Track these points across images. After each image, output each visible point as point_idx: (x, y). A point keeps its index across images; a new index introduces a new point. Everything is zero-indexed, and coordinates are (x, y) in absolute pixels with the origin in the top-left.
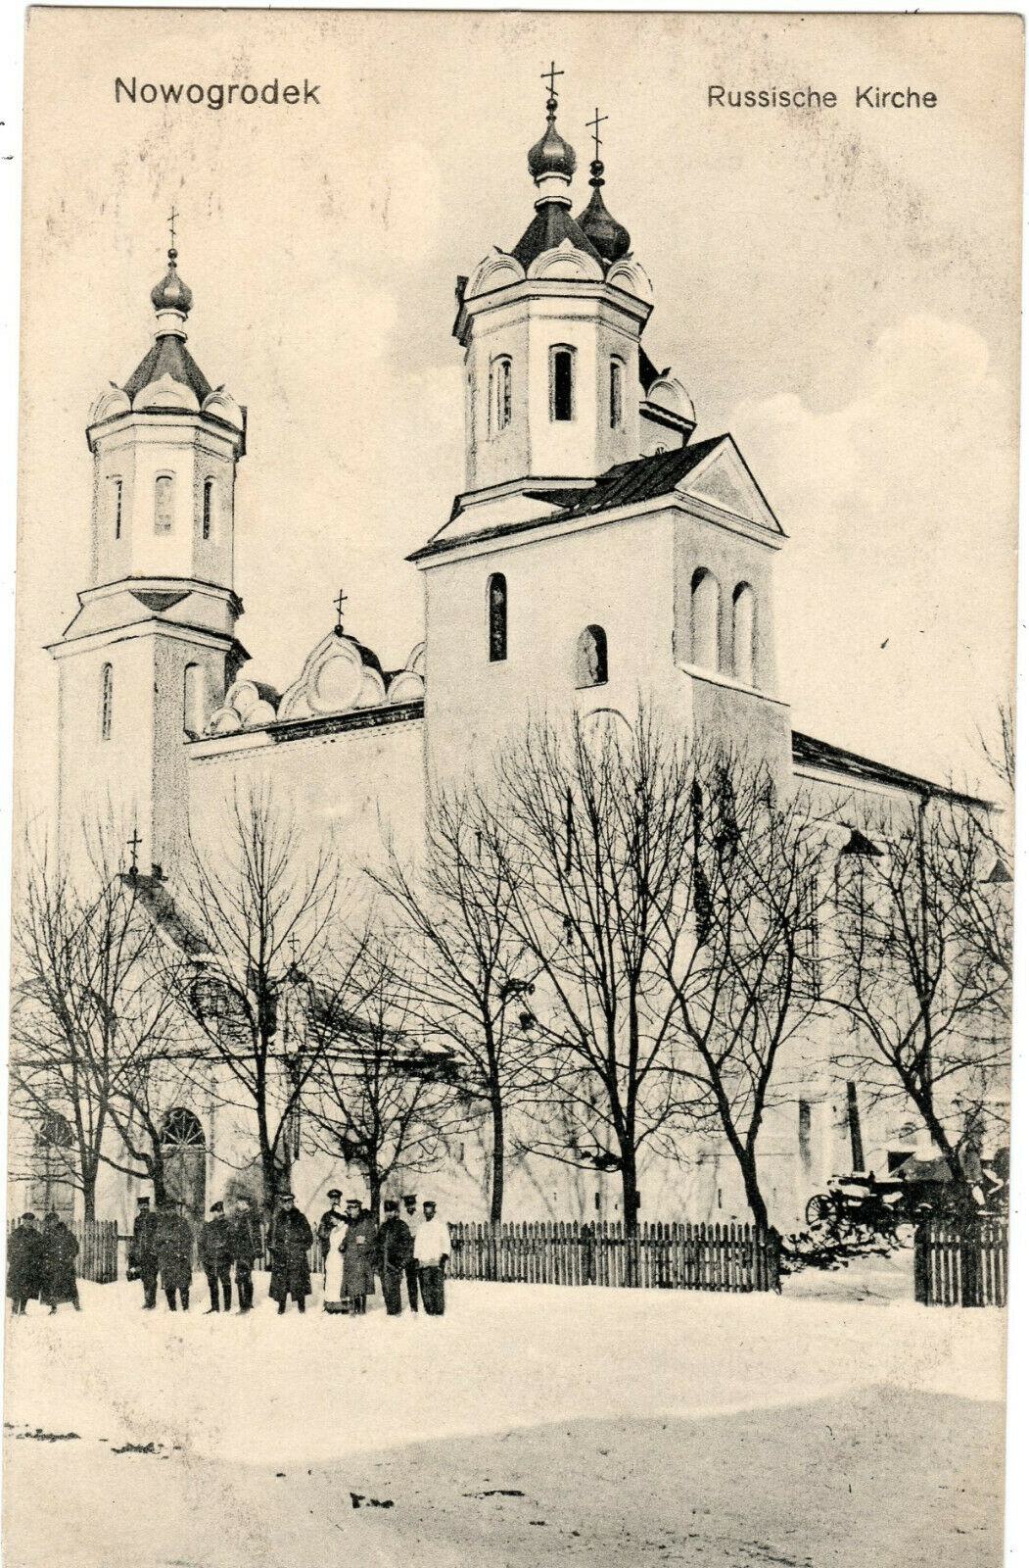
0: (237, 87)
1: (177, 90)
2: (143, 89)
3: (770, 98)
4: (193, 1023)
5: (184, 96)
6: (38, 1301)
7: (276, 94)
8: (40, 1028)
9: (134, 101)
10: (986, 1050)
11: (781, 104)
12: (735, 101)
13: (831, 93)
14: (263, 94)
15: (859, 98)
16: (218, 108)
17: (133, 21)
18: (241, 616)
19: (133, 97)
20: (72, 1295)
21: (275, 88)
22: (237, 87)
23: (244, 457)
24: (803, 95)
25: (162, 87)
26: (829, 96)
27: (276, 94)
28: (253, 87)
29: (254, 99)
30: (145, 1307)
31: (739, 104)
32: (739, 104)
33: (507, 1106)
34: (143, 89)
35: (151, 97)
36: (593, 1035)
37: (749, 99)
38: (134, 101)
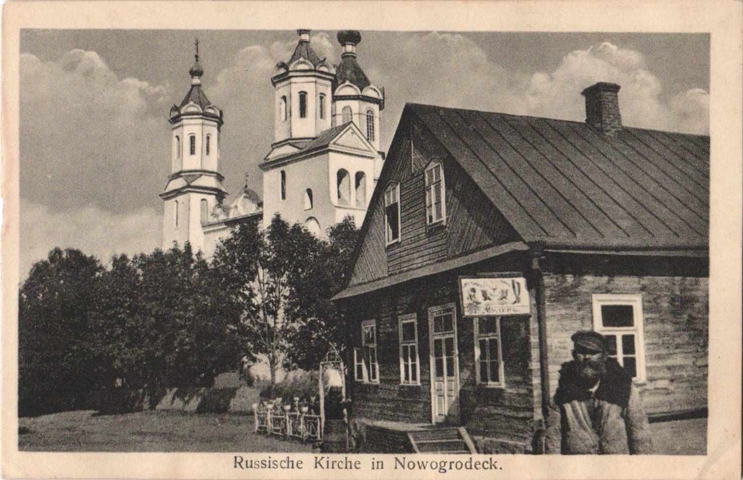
1: (425, 464)
2: (408, 464)
3: (267, 464)
5: (428, 467)
6: (130, 257)
7: (471, 466)
9: (404, 468)
10: (234, 214)
11: (273, 467)
12: (249, 465)
15: (316, 463)
17: (734, 436)
19: (403, 467)
20: (115, 261)
22: (453, 462)
24: (487, 463)
25: (418, 462)
26: (478, 463)
27: (471, 466)
29: (461, 467)
30: (278, 216)
31: (471, 468)
32: (451, 463)
34: (408, 464)
37: (275, 464)
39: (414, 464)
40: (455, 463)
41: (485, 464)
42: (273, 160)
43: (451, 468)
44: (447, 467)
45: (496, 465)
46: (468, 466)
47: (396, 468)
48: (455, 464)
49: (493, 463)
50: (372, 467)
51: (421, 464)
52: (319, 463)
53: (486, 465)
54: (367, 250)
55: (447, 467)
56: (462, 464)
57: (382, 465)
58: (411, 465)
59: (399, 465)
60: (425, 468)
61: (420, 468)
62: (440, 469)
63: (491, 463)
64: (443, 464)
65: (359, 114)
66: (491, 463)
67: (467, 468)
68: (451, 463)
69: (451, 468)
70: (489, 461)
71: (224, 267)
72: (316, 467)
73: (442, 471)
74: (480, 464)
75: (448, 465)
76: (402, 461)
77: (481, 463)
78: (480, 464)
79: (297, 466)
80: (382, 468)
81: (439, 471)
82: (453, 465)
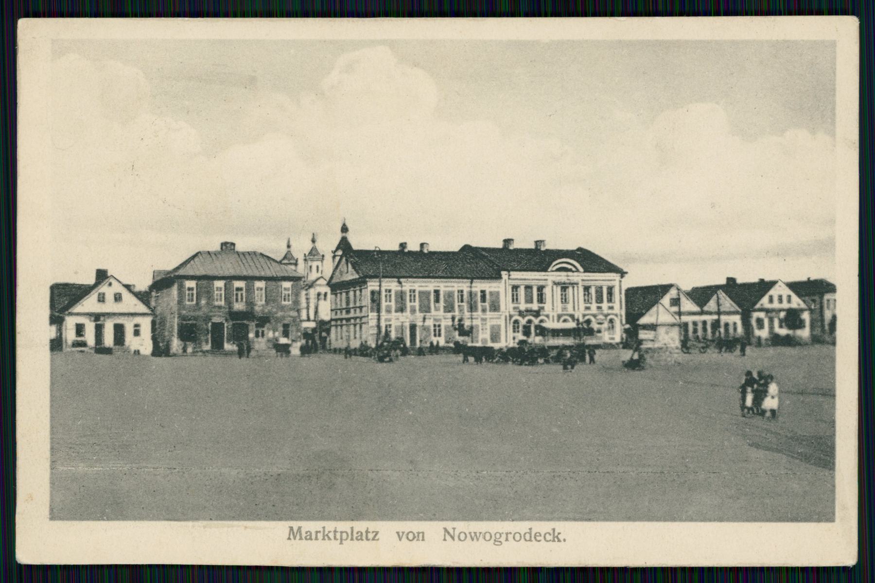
0: (511, 533)
4: (197, 357)
5: (481, 538)
7: (531, 537)
8: (789, 472)
9: (400, 540)
13: (539, 533)
14: (521, 537)
16: (500, 545)
18: (422, 357)
19: (453, 538)
21: (530, 534)
22: (511, 533)
23: (236, 246)
24: (550, 534)
25: (470, 533)
26: (538, 534)
27: (531, 537)
28: (490, 533)
29: (520, 539)
31: (530, 540)
32: (507, 534)
33: (366, 342)
35: (410, 534)
36: (743, 406)
38: (400, 540)
39: (465, 534)
40: (513, 533)
41: (547, 535)
42: (465, 280)
43: (507, 540)
44: (503, 539)
45: (559, 536)
46: (344, 535)
47: (445, 540)
48: (512, 535)
49: (326, 533)
50: (443, 538)
51: (473, 535)
52: (327, 535)
53: (548, 537)
54: (762, 350)
55: (503, 539)
56: (465, 534)
57: (423, 537)
58: (462, 536)
59: (448, 537)
60: (478, 540)
61: (473, 539)
62: (495, 541)
63: (554, 534)
64: (498, 536)
65: (472, 318)
66: (554, 534)
67: (526, 540)
68: (507, 534)
69: (507, 540)
70: (551, 532)
71: (460, 264)
72: (378, 540)
73: (496, 543)
74: (540, 536)
75: (504, 536)
76: (451, 532)
77: (543, 535)
78: (540, 536)
79: (535, 538)
80: (423, 540)
81: (494, 544)
82: (510, 537)
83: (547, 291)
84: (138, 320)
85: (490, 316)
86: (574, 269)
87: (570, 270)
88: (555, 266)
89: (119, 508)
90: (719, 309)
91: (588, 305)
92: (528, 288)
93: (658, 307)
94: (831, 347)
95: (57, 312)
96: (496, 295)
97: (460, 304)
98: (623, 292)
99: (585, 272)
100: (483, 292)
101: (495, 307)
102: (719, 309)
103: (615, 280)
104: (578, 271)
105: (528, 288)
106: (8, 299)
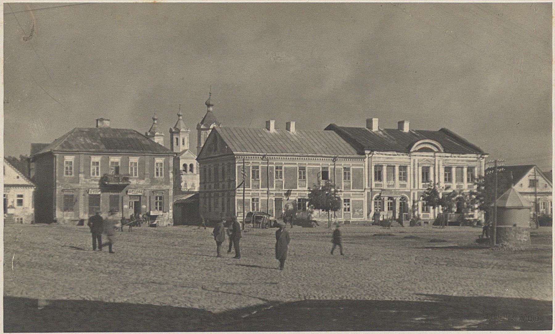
83: (409, 171)
84: (20, 191)
85: (262, 192)
86: (435, 150)
87: (431, 151)
88: (417, 146)
89: (264, 255)
90: (366, 189)
91: (449, 184)
92: (391, 168)
93: (31, 186)
94: (16, 294)
95: (121, 182)
96: (359, 174)
97: (378, 182)
98: (107, 150)
99: (445, 152)
100: (347, 169)
101: (358, 184)
102: (366, 189)
103: (414, 160)
104: (439, 151)
105: (391, 168)
106: (56, 169)
